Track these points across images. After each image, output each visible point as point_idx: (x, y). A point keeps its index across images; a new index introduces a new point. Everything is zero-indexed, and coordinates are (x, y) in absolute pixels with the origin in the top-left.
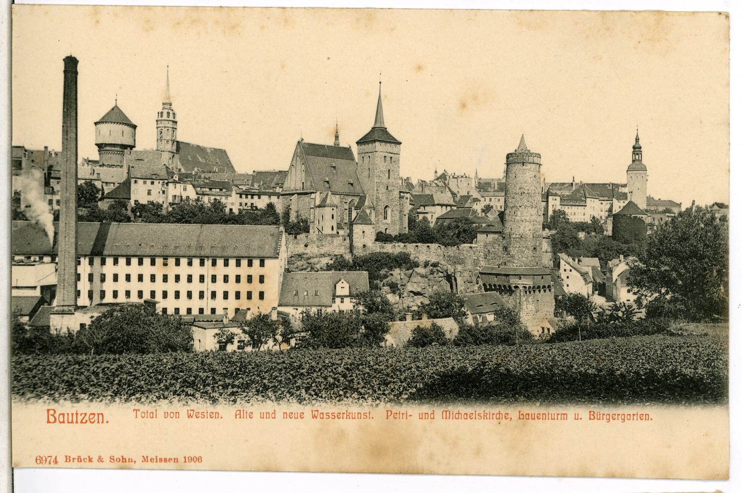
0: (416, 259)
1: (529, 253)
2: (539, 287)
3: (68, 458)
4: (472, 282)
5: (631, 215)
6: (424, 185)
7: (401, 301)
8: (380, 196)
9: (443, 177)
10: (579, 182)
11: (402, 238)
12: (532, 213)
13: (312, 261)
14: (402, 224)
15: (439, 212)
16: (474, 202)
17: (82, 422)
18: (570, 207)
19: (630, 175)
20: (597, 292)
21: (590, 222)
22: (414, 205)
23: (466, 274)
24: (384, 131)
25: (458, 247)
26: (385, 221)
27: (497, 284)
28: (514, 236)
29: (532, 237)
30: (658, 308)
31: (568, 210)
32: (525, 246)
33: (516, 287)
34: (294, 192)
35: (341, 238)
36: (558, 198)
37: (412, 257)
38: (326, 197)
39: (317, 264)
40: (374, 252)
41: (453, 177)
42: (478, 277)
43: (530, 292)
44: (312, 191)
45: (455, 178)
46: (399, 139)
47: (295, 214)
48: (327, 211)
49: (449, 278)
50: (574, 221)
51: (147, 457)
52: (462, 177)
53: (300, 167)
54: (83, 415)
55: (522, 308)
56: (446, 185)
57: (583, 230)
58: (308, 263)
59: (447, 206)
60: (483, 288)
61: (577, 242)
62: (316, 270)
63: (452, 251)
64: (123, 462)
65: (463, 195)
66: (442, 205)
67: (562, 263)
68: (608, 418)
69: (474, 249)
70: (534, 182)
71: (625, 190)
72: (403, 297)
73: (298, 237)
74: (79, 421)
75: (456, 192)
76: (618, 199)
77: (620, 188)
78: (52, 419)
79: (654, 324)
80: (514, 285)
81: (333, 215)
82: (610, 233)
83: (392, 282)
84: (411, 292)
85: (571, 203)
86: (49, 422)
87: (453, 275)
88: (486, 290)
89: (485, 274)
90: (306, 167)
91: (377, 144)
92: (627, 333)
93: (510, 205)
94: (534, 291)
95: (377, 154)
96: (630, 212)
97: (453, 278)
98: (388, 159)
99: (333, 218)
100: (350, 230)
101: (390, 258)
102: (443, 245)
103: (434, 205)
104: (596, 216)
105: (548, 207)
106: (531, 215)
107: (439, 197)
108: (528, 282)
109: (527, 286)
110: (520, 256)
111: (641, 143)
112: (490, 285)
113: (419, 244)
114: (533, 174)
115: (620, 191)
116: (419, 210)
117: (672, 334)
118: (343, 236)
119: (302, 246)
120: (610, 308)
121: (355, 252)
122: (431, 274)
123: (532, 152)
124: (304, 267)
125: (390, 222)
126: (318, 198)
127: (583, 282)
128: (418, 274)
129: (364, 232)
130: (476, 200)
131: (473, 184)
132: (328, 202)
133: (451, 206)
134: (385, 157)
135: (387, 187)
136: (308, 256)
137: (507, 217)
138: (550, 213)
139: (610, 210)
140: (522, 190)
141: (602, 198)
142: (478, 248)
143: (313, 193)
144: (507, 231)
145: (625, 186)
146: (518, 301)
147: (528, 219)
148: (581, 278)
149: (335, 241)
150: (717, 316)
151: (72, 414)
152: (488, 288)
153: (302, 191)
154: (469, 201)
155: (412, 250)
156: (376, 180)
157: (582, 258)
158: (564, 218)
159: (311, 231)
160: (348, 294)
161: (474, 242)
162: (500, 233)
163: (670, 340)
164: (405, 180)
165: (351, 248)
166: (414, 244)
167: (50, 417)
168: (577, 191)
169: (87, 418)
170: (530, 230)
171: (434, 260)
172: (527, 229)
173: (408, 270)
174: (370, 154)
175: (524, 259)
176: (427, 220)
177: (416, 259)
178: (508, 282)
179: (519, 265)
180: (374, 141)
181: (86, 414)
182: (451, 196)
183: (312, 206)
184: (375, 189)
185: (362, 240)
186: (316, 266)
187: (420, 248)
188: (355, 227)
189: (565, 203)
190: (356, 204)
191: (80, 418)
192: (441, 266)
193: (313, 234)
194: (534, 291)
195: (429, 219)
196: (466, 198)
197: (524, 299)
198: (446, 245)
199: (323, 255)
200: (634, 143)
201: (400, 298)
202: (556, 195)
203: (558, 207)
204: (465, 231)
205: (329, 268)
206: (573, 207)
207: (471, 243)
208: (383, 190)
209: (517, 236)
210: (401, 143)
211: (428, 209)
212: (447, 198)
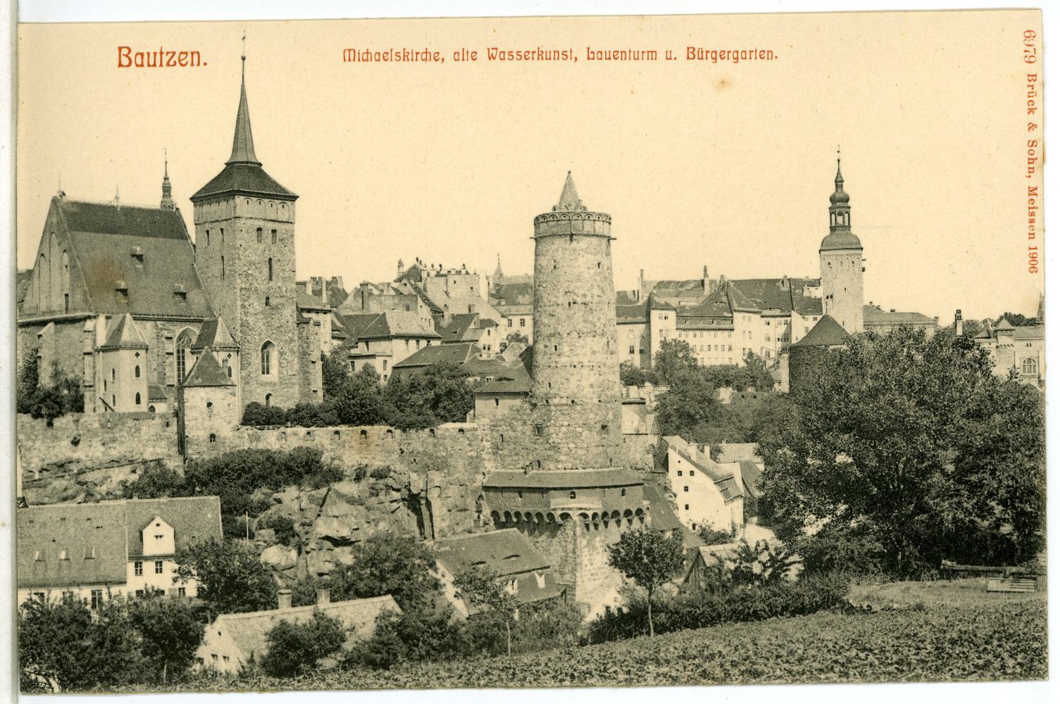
0: (336, 462)
1: (591, 438)
2: (616, 513)
3: (1034, 78)
4: (466, 510)
5: (827, 346)
6: (366, 294)
7: (302, 562)
8: (251, 319)
9: (414, 274)
10: (718, 279)
11: (304, 416)
12: (595, 349)
13: (89, 477)
14: (306, 381)
15: (401, 351)
16: (483, 328)
17: (168, 64)
18: (698, 333)
19: (828, 261)
20: (755, 519)
21: (742, 364)
22: (343, 339)
23: (453, 491)
24: (256, 169)
25: (432, 431)
26: (265, 378)
27: (523, 511)
28: (556, 401)
29: (596, 401)
30: (822, 552)
31: (691, 339)
32: (581, 422)
33: (565, 516)
34: (48, 317)
35: (158, 421)
36: (672, 315)
37: (325, 459)
38: (119, 329)
39: (102, 483)
40: (235, 450)
41: (438, 275)
42: (481, 497)
43: (596, 526)
44: (87, 313)
45: (442, 276)
46: (296, 193)
47: (50, 370)
48: (126, 360)
49: (415, 502)
50: (707, 363)
51: (1036, 194)
52: (459, 273)
53: (59, 259)
54: (170, 55)
55: (581, 564)
56: (421, 293)
57: (728, 383)
58: (79, 483)
59: (418, 338)
60: (492, 523)
61: (712, 411)
62: (99, 497)
63: (419, 440)
64: (1029, 159)
65: (457, 312)
66: (407, 338)
67: (673, 457)
68: (714, 57)
69: (468, 434)
70: (598, 278)
71: (817, 293)
72: (308, 553)
73: (57, 422)
74: (164, 63)
75: (442, 307)
76: (803, 313)
77: (805, 288)
78: (125, 61)
79: (815, 588)
80: (559, 512)
81: (137, 368)
82: (784, 387)
83: (280, 517)
84: (327, 538)
85: (701, 325)
86: (120, 65)
87: (423, 494)
88: (500, 525)
89: (495, 489)
90: (71, 259)
91: (240, 200)
92: (755, 612)
93: (546, 331)
94: (606, 524)
95: (239, 223)
96: (827, 340)
97: (423, 502)
98: (267, 234)
99: (138, 375)
100: (179, 402)
101: (274, 464)
102: (399, 427)
103: (389, 338)
104: (756, 351)
105: (649, 335)
106: (594, 353)
107: (398, 320)
108: (591, 503)
109: (590, 513)
110: (572, 446)
111: (847, 188)
112: (507, 514)
113: (343, 428)
114: (593, 260)
115: (806, 294)
116: (354, 352)
117: (850, 610)
118: (162, 416)
119: (66, 443)
120: (735, 556)
121: (190, 451)
122: (372, 494)
123: (590, 209)
124: (70, 492)
125: (276, 380)
126: (101, 329)
127: (720, 498)
128: (340, 496)
129: (209, 405)
130: (487, 324)
131: (483, 291)
132: (126, 336)
133: (428, 338)
134: (259, 229)
135: (268, 298)
136: (81, 466)
137: (540, 359)
138: (656, 347)
139: (786, 337)
140: (570, 298)
141: (765, 312)
142: (479, 432)
143: (89, 317)
144: (541, 390)
145: (815, 283)
146: (570, 547)
147: (585, 360)
148: (716, 489)
149: (144, 429)
150: (949, 563)
151: (155, 54)
152: (503, 520)
153: (65, 315)
154: (472, 326)
155: (326, 442)
156: (240, 283)
157: (723, 445)
158: (686, 357)
159: (88, 407)
160: (170, 549)
161: (468, 419)
162: (526, 394)
163: (854, 625)
164: (328, 283)
165: (182, 443)
166: (331, 428)
167: (123, 58)
168: (714, 298)
169: (176, 58)
170: (591, 386)
171: (377, 463)
172: (585, 383)
173: (317, 487)
174: (223, 225)
175: (580, 452)
176: (374, 372)
177: (336, 462)
178: (547, 504)
179: (570, 466)
180: (232, 194)
181: (174, 53)
182: (429, 316)
183: (88, 349)
184: (239, 303)
185: (207, 423)
186: (98, 488)
187: (344, 437)
188: (188, 393)
189: (687, 325)
190: (194, 340)
191: (166, 58)
192: (396, 476)
193: (91, 417)
194: (606, 524)
195: (379, 369)
196: (463, 320)
197: (584, 542)
198: (405, 427)
199: (116, 463)
200: (831, 189)
201: (299, 553)
202: (667, 307)
203: (673, 335)
204: (450, 393)
205: (129, 491)
206: (705, 333)
207: (463, 420)
208: (257, 305)
209: (564, 401)
210: (294, 198)
211: (375, 347)
212: (421, 320)
